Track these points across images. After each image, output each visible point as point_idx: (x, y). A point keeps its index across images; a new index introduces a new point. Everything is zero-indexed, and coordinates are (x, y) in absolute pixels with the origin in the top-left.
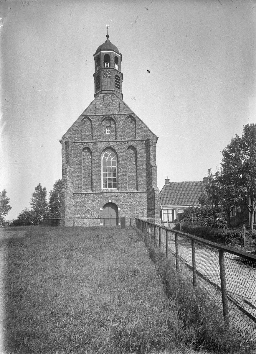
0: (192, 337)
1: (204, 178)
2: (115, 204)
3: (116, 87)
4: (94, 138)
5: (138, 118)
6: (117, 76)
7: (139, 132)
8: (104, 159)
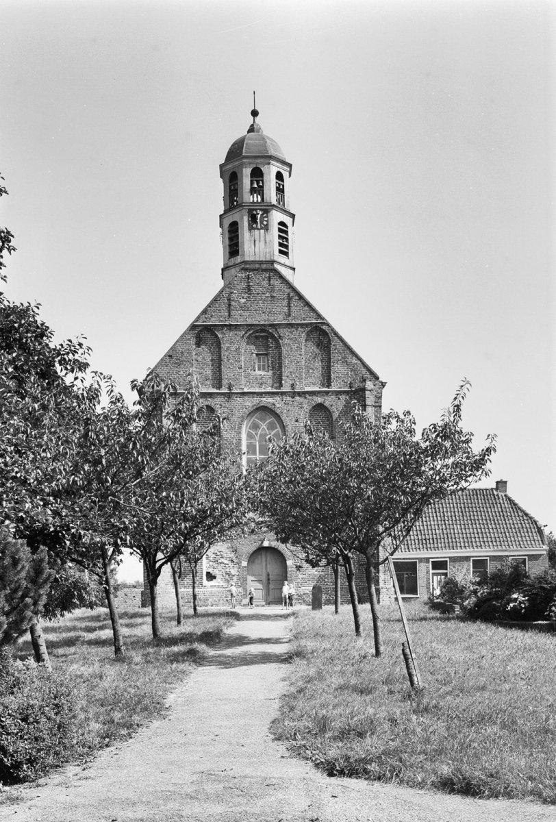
0: (467, 648)
1: (497, 483)
2: (282, 554)
3: (281, 252)
4: (225, 382)
5: (336, 334)
6: (282, 223)
7: (338, 369)
8: (250, 436)
